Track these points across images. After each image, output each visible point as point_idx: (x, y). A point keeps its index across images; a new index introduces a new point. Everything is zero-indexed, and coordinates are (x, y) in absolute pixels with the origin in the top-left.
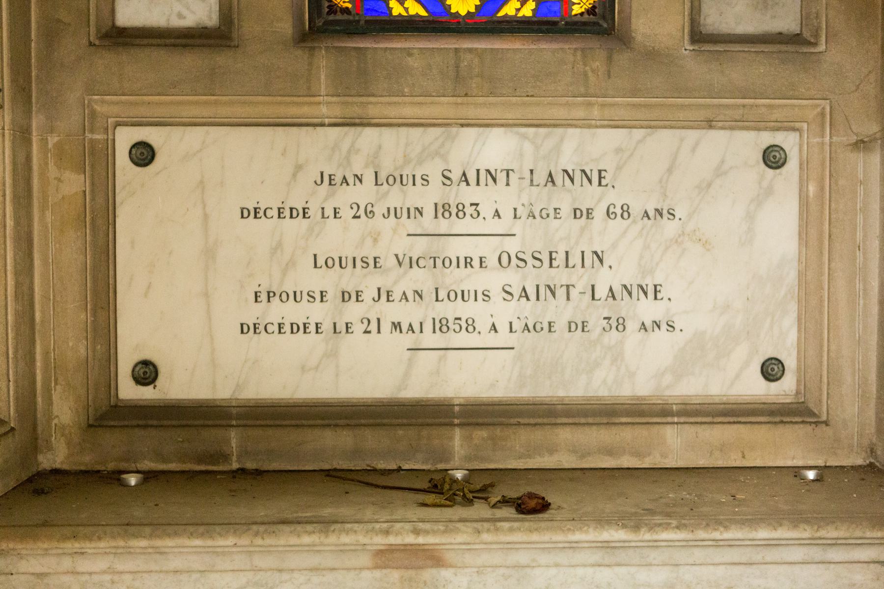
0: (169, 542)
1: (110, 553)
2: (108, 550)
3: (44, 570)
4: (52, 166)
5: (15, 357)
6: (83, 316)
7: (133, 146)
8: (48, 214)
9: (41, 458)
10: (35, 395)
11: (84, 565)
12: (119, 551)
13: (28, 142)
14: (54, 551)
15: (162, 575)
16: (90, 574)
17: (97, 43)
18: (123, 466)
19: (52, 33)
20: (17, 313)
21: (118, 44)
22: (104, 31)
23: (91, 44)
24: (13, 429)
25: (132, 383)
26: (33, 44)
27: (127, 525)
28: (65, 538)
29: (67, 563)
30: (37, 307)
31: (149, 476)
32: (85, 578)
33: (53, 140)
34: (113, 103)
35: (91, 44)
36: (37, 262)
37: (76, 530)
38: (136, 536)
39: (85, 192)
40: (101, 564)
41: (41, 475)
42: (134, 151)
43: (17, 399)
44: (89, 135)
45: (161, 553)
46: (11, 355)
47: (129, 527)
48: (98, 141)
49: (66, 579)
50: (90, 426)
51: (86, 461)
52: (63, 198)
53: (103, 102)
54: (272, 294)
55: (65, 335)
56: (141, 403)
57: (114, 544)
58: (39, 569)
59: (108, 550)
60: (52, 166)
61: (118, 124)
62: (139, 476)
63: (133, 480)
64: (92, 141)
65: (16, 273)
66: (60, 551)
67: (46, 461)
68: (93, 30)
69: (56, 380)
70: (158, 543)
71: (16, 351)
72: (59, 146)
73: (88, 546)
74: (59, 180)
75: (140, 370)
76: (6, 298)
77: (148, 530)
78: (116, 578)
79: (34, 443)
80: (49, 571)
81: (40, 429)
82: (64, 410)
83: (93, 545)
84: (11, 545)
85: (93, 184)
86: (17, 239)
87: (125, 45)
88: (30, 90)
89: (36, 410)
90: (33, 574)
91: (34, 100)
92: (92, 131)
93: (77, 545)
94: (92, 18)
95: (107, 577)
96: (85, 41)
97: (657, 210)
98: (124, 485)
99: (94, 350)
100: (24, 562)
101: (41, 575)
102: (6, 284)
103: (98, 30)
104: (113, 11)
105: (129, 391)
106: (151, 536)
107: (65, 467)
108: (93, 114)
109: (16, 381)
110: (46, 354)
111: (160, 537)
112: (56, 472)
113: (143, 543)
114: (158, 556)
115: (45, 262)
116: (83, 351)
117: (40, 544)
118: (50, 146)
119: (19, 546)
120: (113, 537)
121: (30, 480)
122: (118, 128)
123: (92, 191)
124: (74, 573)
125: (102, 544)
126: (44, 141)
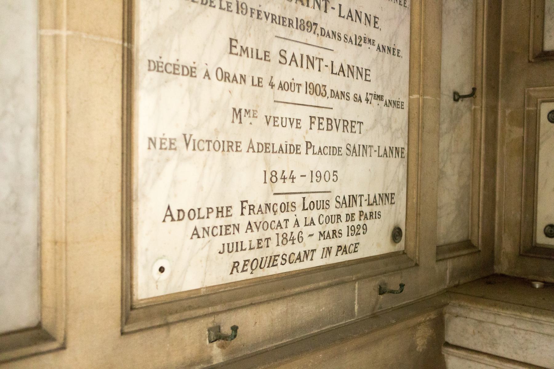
0: (543, 318)
1: (512, 317)
2: (512, 316)
3: (481, 319)
4: (507, 124)
5: (483, 216)
6: (519, 199)
7: (550, 113)
8: (505, 147)
9: (495, 267)
10: (494, 237)
11: (500, 321)
12: (517, 317)
13: (496, 113)
14: (485, 311)
15: (541, 335)
16: (504, 326)
17: (533, 60)
18: (536, 277)
19: (510, 58)
20: (484, 195)
21: (544, 60)
22: (537, 54)
23: (529, 62)
24: (480, 251)
25: (544, 236)
26: (501, 65)
27: (523, 305)
28: (491, 306)
29: (492, 318)
30: (497, 194)
31: (546, 285)
32: (502, 327)
33: (508, 112)
34: (540, 91)
35: (529, 62)
36: (498, 172)
37: (506, 304)
38: (526, 311)
39: (523, 137)
40: (508, 322)
41: (496, 275)
42: (550, 115)
43: (483, 237)
44: (527, 108)
45: (540, 324)
46: (481, 215)
47: (524, 307)
48: (532, 111)
49: (492, 326)
50: (520, 255)
51: (518, 272)
52: (512, 140)
53: (535, 91)
54: (210, 210)
55: (509, 207)
56: (542, 246)
57: (514, 313)
58: (478, 318)
59: (512, 316)
60: (507, 124)
61: (544, 102)
62: (542, 284)
63: (537, 285)
64: (528, 111)
65: (485, 176)
66: (488, 311)
67: (498, 269)
68: (531, 54)
69: (505, 230)
70: (537, 317)
71: (483, 214)
72: (511, 114)
73: (502, 312)
74: (510, 131)
75: (549, 229)
76: (479, 188)
77: (532, 310)
78: (516, 331)
79: (491, 260)
80: (484, 320)
81: (496, 252)
82: (507, 246)
83: (504, 311)
84: (466, 304)
85: (528, 133)
86: (486, 161)
87: (548, 60)
88: (498, 88)
89: (493, 244)
90: (476, 320)
91: (500, 92)
92: (529, 106)
93: (496, 310)
94: (531, 49)
95: (512, 330)
96: (526, 61)
97: (267, 205)
98: (533, 287)
99: (525, 217)
100: (472, 313)
101: (480, 321)
102: (480, 181)
103: (534, 54)
104: (542, 44)
105: (541, 239)
106: (533, 313)
107: (507, 274)
108: (530, 97)
109: (483, 228)
110: (500, 217)
111: (537, 314)
112: (503, 275)
113: (529, 316)
114: (538, 324)
115: (502, 171)
116: (518, 216)
117: (479, 306)
118: (507, 114)
119: (469, 305)
120: (514, 310)
121: (488, 277)
122: (542, 104)
123: (527, 136)
124: (495, 323)
125: (508, 312)
126: (504, 112)
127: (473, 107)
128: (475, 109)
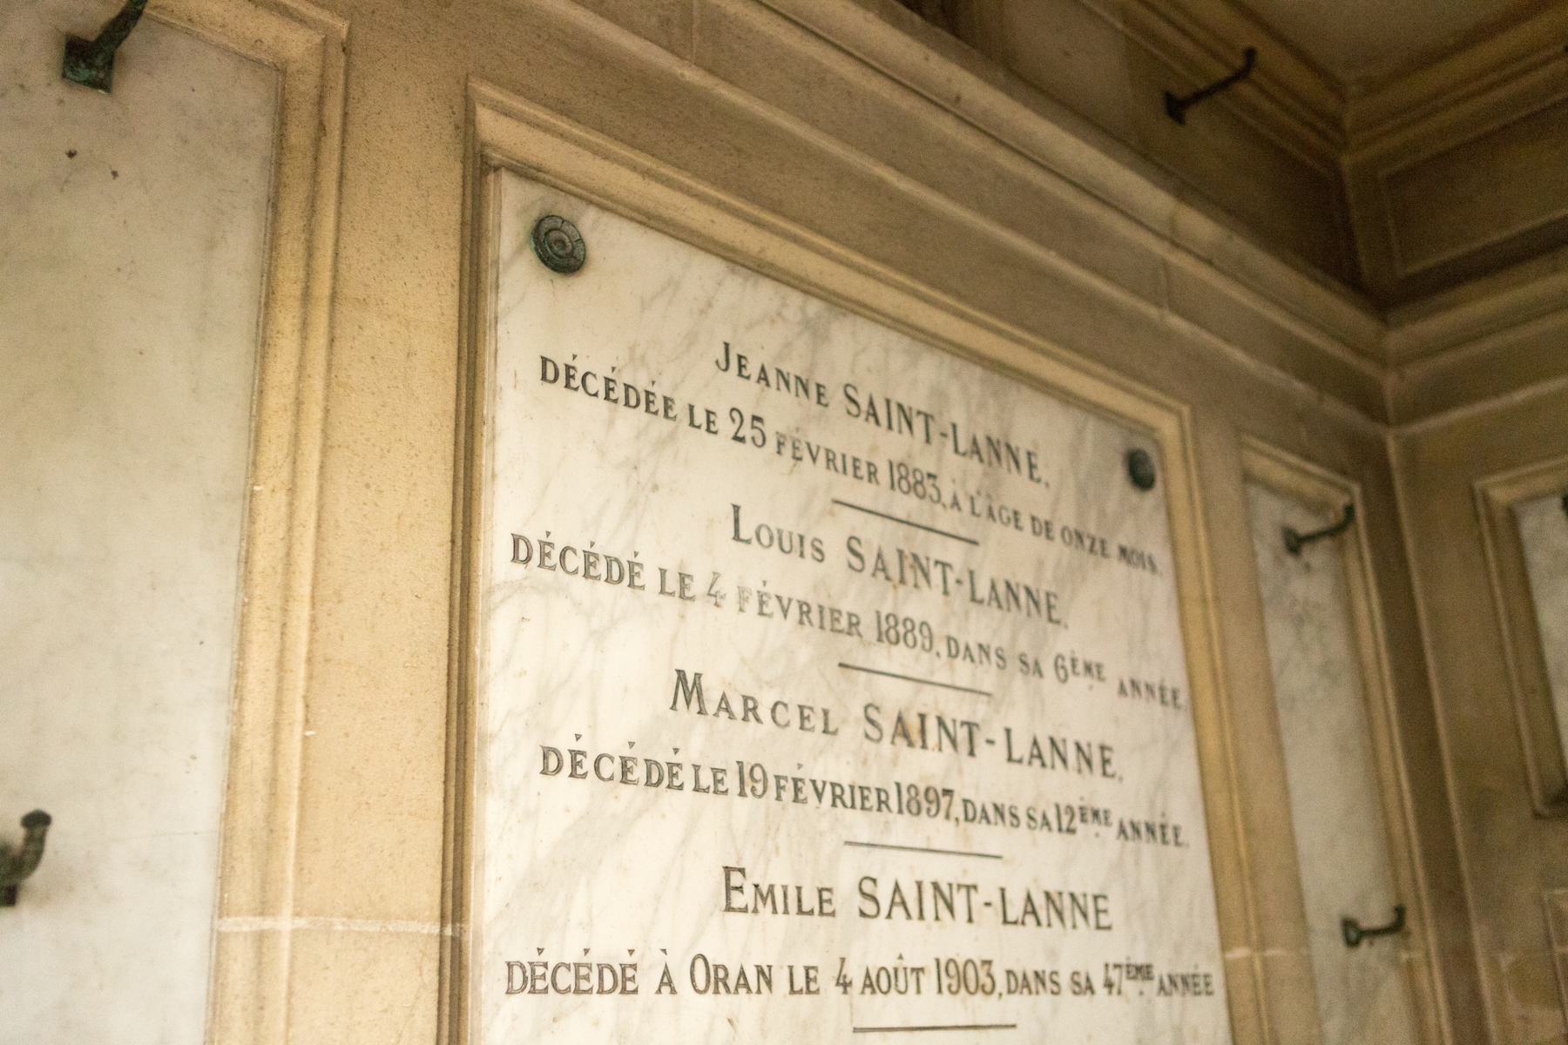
23: (1537, 815)
33: (1506, 960)
127: (1404, 956)
128: (1410, 963)
